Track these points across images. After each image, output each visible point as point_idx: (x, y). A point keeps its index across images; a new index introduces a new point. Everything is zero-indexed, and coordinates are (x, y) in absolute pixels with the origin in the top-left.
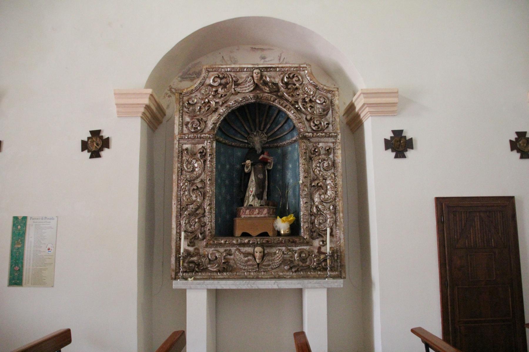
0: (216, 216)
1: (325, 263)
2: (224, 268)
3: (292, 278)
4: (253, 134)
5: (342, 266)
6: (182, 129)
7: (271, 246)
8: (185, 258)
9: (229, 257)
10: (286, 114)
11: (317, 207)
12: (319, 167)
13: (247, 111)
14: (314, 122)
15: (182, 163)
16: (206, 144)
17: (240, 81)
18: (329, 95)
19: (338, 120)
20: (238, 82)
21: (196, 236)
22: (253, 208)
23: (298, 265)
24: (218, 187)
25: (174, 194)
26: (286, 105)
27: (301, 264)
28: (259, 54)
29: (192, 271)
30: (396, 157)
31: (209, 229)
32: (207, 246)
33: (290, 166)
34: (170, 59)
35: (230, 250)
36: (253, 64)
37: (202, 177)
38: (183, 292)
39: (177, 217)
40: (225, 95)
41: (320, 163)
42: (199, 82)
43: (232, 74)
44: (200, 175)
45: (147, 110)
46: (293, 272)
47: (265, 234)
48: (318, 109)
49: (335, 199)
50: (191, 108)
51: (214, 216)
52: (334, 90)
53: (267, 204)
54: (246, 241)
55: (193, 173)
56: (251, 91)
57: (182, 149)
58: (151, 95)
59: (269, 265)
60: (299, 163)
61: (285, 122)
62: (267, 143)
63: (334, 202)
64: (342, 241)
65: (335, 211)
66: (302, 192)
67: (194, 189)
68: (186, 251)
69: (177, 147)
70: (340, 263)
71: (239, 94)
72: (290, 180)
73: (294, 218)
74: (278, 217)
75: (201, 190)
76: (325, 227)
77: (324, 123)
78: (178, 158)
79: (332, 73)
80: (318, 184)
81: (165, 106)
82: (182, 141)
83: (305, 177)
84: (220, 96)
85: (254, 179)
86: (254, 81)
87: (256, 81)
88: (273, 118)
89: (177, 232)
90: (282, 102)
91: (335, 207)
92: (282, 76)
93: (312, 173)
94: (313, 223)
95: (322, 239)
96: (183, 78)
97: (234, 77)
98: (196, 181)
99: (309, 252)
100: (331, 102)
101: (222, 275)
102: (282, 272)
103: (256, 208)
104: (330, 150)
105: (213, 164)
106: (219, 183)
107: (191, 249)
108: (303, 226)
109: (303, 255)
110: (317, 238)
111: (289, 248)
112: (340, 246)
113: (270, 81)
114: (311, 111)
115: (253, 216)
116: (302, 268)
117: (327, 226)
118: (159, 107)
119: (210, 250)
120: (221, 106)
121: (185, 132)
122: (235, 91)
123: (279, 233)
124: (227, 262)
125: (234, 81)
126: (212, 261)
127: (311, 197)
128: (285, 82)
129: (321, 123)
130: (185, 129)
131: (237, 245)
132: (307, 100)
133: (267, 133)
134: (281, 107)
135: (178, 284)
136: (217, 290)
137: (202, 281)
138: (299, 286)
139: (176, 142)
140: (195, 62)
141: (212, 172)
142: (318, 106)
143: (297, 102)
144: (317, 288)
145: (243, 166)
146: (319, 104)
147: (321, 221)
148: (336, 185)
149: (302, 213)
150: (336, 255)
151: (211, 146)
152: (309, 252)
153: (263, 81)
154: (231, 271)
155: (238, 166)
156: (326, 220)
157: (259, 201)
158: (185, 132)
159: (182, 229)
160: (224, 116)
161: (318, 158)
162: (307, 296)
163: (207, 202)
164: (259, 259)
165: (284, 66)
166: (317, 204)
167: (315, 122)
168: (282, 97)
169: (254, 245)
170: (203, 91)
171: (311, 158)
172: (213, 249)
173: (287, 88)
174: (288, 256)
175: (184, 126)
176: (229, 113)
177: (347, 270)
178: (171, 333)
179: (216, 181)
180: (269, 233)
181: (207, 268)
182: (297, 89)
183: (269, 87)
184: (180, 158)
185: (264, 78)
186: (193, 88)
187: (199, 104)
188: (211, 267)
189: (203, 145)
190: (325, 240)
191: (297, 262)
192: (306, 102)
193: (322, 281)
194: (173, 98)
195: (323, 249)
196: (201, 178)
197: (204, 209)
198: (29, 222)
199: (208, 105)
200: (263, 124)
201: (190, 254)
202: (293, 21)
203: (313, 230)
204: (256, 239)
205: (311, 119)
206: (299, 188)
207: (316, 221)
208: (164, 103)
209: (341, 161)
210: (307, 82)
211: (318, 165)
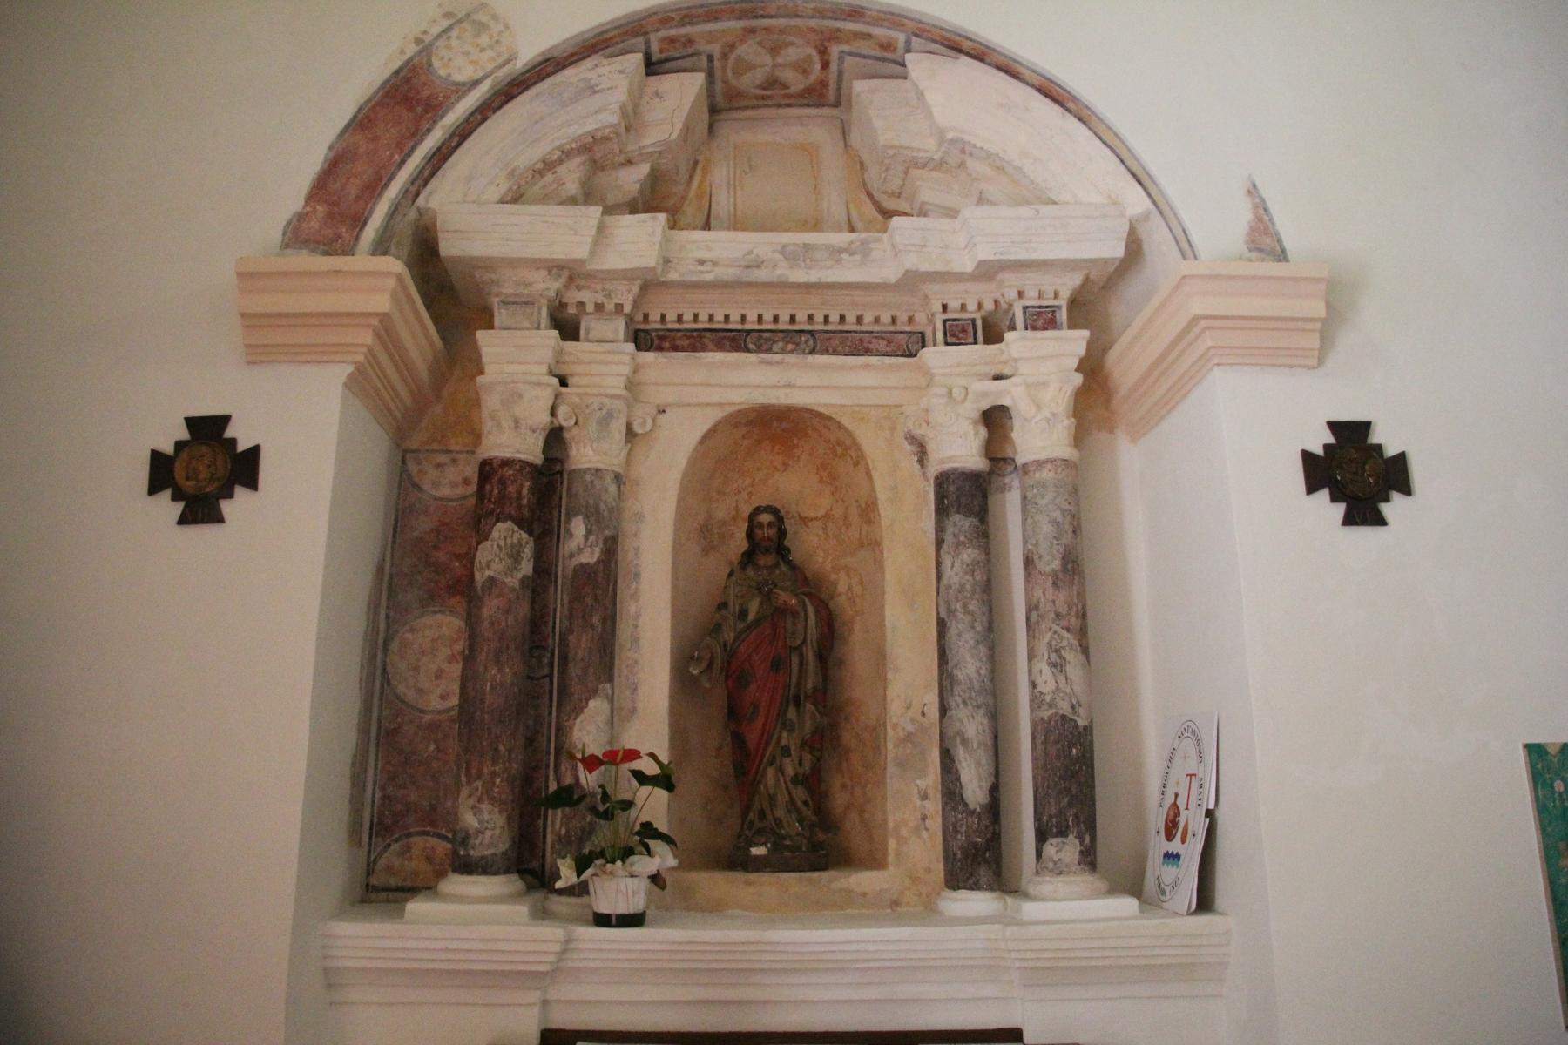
30: (1349, 520)
45: (383, 343)
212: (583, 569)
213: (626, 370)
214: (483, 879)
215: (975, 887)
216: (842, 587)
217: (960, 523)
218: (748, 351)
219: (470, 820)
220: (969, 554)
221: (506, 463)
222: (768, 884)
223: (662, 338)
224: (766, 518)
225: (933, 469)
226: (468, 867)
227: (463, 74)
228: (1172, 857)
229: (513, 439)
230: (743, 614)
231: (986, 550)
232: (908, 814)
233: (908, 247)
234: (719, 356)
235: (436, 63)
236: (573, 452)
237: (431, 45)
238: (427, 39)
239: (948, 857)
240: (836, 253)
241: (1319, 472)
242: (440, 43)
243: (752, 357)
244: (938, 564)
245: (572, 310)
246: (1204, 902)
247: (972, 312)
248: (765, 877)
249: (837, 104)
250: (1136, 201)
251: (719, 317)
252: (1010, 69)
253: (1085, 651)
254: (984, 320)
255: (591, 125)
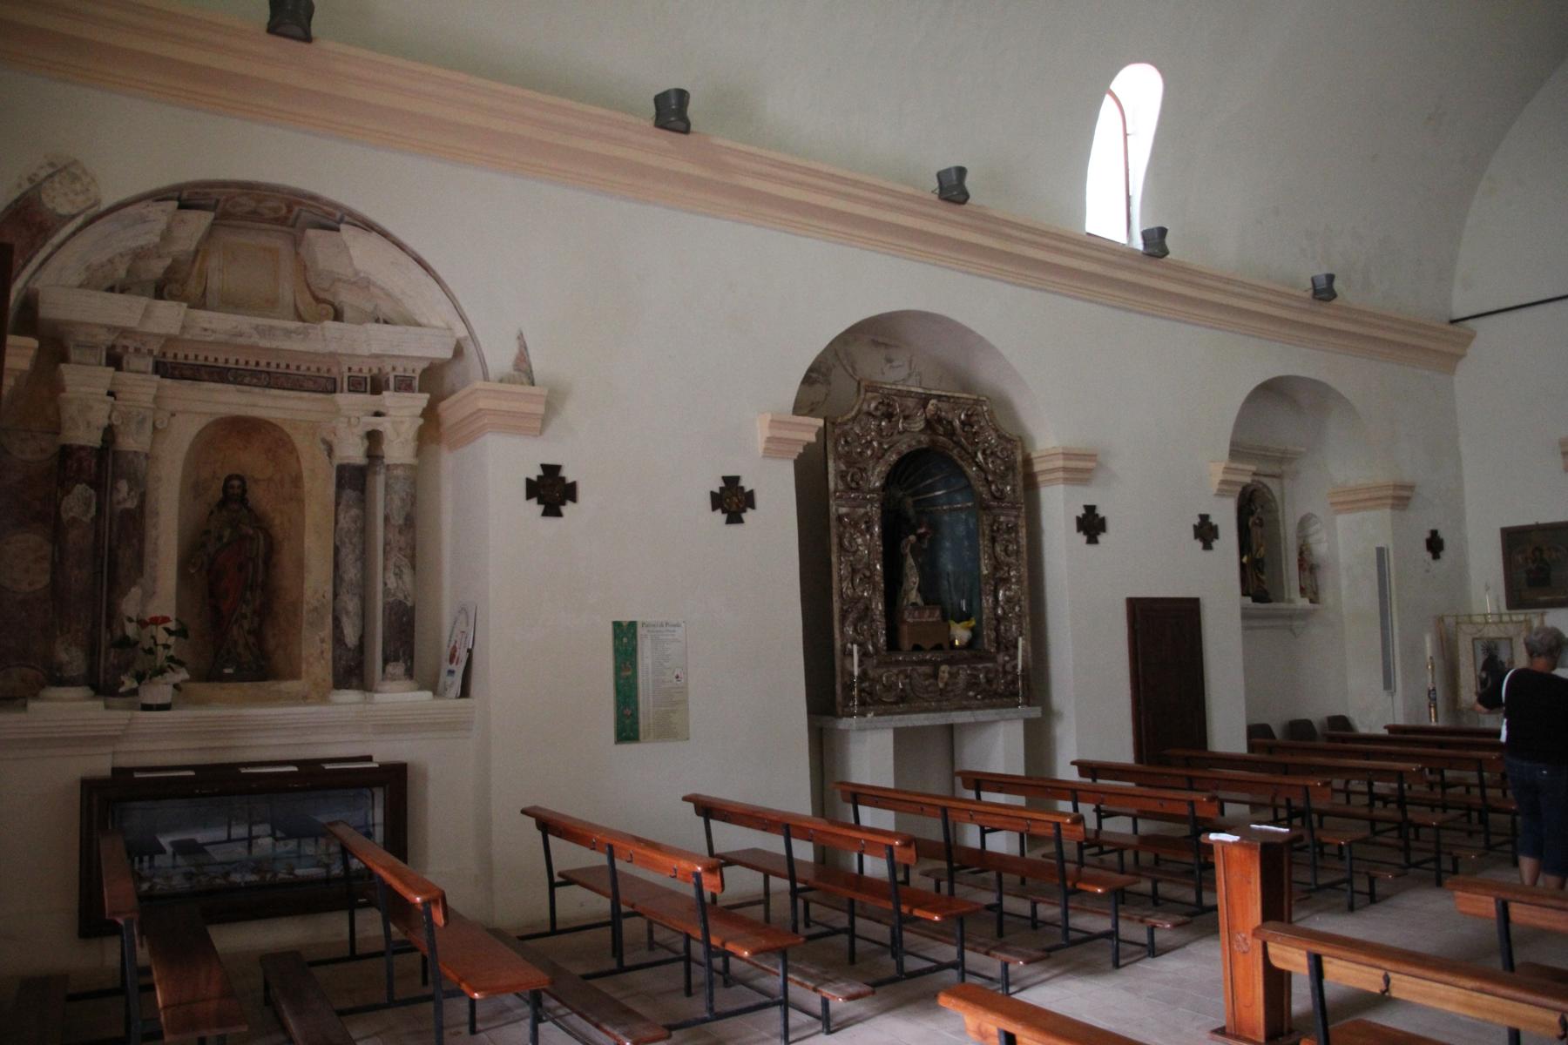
30: (545, 514)
33: (948, 544)
79: (1006, 405)
198: (641, 631)
212: (128, 511)
213: (153, 391)
214: (72, 689)
215: (349, 688)
216: (277, 522)
217: (349, 494)
218: (229, 382)
219: (63, 657)
220: (354, 512)
221: (82, 448)
222: (234, 689)
223: (174, 368)
224: (236, 483)
225: (336, 462)
226: (61, 683)
227: (64, 209)
228: (451, 672)
229: (86, 435)
230: (220, 538)
231: (364, 509)
232: (315, 650)
233: (331, 339)
234: (212, 385)
235: (45, 198)
236: (120, 439)
237: (40, 184)
238: (38, 180)
239: (335, 674)
240: (288, 333)
241: (534, 489)
242: (47, 184)
243: (231, 387)
244: (336, 515)
245: (119, 350)
246: (465, 692)
247: (365, 373)
248: (232, 685)
249: (293, 226)
250: (461, 331)
251: (211, 359)
252: (401, 246)
253: (414, 567)
254: (373, 379)
255: (142, 242)
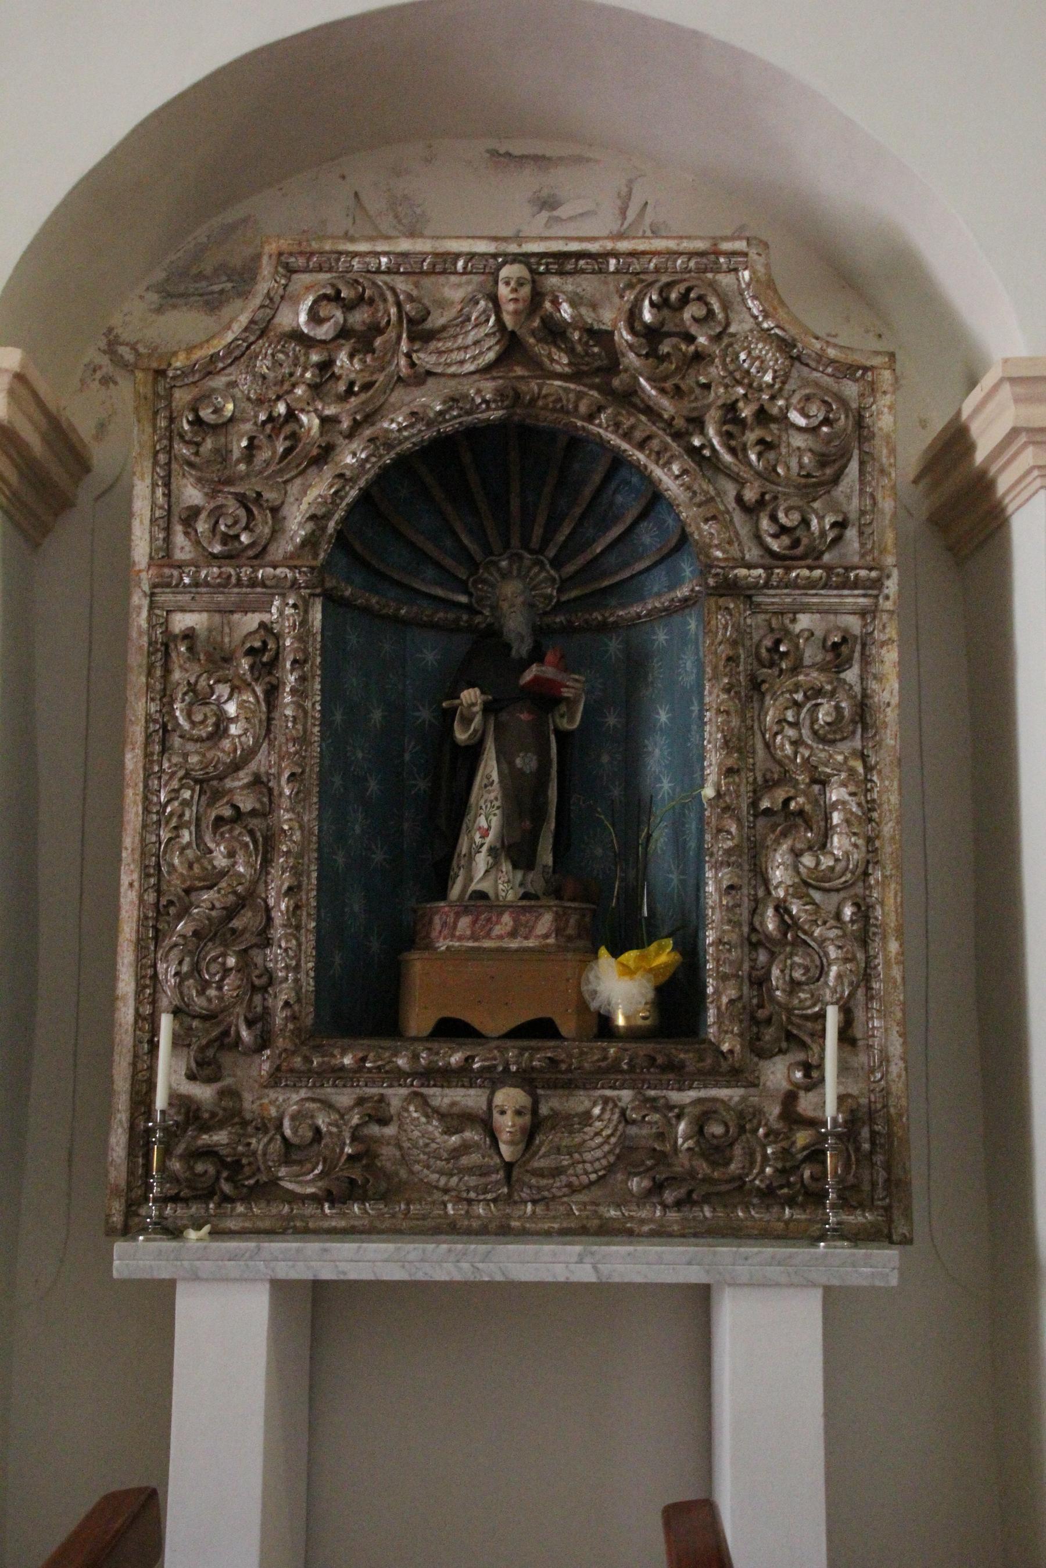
0: (319, 940)
1: (817, 1168)
2: (352, 1182)
3: (661, 1233)
4: (495, 564)
5: (897, 1186)
6: (167, 540)
7: (570, 1085)
8: (172, 1135)
9: (375, 1130)
10: (647, 479)
11: (781, 909)
12: (795, 725)
13: (467, 458)
14: (774, 518)
15: (166, 698)
16: (280, 612)
17: (436, 320)
18: (851, 389)
19: (887, 505)
20: (429, 325)
21: (226, 1033)
22: (491, 907)
23: (692, 1174)
24: (333, 806)
25: (130, 840)
26: (649, 438)
27: (703, 1168)
28: (526, 182)
29: (207, 1194)
31: (287, 1004)
32: (275, 1079)
34: (103, 199)
35: (382, 1099)
36: (495, 239)
37: (261, 762)
38: (158, 1299)
39: (140, 945)
40: (367, 386)
41: (798, 705)
42: (244, 319)
43: (402, 284)
44: (250, 753)
46: (665, 1207)
47: (542, 1029)
48: (798, 451)
49: (866, 874)
50: (209, 444)
51: (309, 941)
52: (876, 361)
53: (557, 893)
54: (456, 1059)
55: (215, 746)
56: (486, 370)
57: (166, 632)
58: (19, 377)
59: (557, 1172)
60: (702, 703)
61: (643, 516)
62: (560, 607)
63: (859, 889)
64: (896, 1068)
65: (865, 929)
66: (715, 837)
67: (219, 820)
68: (177, 1099)
69: (144, 625)
70: (888, 1167)
71: (431, 382)
72: (661, 782)
73: (677, 957)
74: (603, 951)
75: (254, 823)
76: (816, 999)
77: (821, 518)
78: (149, 674)
79: (873, 279)
80: (786, 802)
81: (84, 427)
82: (165, 597)
83: (730, 772)
84: (342, 387)
85: (495, 776)
86: (499, 320)
87: (508, 320)
88: (588, 492)
89: (138, 1015)
90: (627, 423)
91: (864, 912)
92: (630, 296)
93: (759, 746)
94: (760, 981)
95: (801, 1056)
96: (171, 295)
97: (411, 298)
98: (229, 783)
99: (741, 1115)
100: (860, 423)
101: (343, 1215)
102: (618, 1206)
103: (502, 908)
104: (844, 649)
105: (308, 704)
106: (336, 786)
107: (203, 1093)
108: (716, 991)
109: (716, 1129)
110: (781, 1051)
111: (652, 1093)
112: (886, 1093)
113: (578, 318)
114: (761, 466)
115: (487, 944)
116: (705, 1189)
117: (828, 997)
118: (58, 432)
119: (289, 1101)
120: (350, 435)
121: (179, 555)
122: (413, 365)
123: (604, 1027)
124: (366, 1155)
125: (410, 321)
126: (299, 1147)
127: (753, 860)
128: (646, 326)
129: (805, 522)
130: (180, 539)
131: (414, 1075)
132: (746, 412)
133: (557, 563)
134: (625, 446)
135: (137, 1258)
136: (318, 1288)
137: (249, 1245)
138: (694, 1275)
139: (139, 600)
140: (232, 215)
141: (303, 740)
142: (798, 441)
143: (697, 423)
144: (777, 1285)
145: (449, 715)
146: (799, 429)
147: (798, 974)
148: (870, 807)
149: (711, 936)
150: (865, 1132)
151: (304, 623)
152: (741, 1115)
153: (543, 320)
154: (384, 1197)
155: (425, 714)
156: (823, 971)
157: (519, 875)
158: (179, 555)
159: (164, 1002)
160: (362, 483)
161: (789, 683)
162: (731, 1316)
163: (279, 879)
164: (512, 1143)
165: (641, 246)
166: (781, 893)
167: (781, 515)
168: (628, 398)
169: (493, 1079)
170: (263, 366)
171: (756, 685)
172: (303, 1093)
173: (653, 353)
174: (645, 1131)
175: (178, 528)
176: (385, 470)
177: (918, 1204)
178: (96, 1499)
179: (324, 781)
180: (558, 1022)
181: (275, 1182)
182: (699, 358)
183: (571, 351)
184: (158, 673)
185: (548, 305)
186: (218, 346)
187: (248, 427)
188: (295, 1177)
189: (265, 617)
190: (814, 1060)
191: (684, 1159)
192: (742, 423)
193: (802, 1253)
194: (126, 392)
195: (805, 1104)
196: (253, 766)
197: (268, 910)
199: (287, 430)
200: (541, 519)
201: (197, 1118)
202: (688, 18)
203: (761, 1014)
204: (503, 1050)
205: (761, 503)
206: (701, 819)
207: (775, 972)
208: (82, 417)
209: (895, 701)
210: (749, 324)
211: (790, 716)
